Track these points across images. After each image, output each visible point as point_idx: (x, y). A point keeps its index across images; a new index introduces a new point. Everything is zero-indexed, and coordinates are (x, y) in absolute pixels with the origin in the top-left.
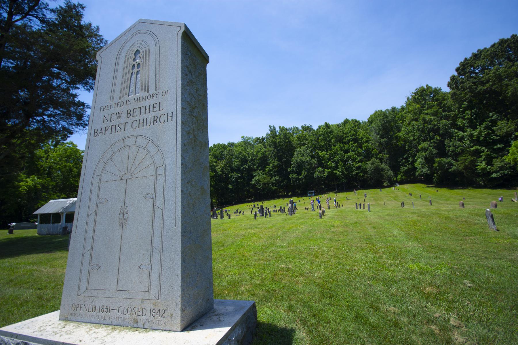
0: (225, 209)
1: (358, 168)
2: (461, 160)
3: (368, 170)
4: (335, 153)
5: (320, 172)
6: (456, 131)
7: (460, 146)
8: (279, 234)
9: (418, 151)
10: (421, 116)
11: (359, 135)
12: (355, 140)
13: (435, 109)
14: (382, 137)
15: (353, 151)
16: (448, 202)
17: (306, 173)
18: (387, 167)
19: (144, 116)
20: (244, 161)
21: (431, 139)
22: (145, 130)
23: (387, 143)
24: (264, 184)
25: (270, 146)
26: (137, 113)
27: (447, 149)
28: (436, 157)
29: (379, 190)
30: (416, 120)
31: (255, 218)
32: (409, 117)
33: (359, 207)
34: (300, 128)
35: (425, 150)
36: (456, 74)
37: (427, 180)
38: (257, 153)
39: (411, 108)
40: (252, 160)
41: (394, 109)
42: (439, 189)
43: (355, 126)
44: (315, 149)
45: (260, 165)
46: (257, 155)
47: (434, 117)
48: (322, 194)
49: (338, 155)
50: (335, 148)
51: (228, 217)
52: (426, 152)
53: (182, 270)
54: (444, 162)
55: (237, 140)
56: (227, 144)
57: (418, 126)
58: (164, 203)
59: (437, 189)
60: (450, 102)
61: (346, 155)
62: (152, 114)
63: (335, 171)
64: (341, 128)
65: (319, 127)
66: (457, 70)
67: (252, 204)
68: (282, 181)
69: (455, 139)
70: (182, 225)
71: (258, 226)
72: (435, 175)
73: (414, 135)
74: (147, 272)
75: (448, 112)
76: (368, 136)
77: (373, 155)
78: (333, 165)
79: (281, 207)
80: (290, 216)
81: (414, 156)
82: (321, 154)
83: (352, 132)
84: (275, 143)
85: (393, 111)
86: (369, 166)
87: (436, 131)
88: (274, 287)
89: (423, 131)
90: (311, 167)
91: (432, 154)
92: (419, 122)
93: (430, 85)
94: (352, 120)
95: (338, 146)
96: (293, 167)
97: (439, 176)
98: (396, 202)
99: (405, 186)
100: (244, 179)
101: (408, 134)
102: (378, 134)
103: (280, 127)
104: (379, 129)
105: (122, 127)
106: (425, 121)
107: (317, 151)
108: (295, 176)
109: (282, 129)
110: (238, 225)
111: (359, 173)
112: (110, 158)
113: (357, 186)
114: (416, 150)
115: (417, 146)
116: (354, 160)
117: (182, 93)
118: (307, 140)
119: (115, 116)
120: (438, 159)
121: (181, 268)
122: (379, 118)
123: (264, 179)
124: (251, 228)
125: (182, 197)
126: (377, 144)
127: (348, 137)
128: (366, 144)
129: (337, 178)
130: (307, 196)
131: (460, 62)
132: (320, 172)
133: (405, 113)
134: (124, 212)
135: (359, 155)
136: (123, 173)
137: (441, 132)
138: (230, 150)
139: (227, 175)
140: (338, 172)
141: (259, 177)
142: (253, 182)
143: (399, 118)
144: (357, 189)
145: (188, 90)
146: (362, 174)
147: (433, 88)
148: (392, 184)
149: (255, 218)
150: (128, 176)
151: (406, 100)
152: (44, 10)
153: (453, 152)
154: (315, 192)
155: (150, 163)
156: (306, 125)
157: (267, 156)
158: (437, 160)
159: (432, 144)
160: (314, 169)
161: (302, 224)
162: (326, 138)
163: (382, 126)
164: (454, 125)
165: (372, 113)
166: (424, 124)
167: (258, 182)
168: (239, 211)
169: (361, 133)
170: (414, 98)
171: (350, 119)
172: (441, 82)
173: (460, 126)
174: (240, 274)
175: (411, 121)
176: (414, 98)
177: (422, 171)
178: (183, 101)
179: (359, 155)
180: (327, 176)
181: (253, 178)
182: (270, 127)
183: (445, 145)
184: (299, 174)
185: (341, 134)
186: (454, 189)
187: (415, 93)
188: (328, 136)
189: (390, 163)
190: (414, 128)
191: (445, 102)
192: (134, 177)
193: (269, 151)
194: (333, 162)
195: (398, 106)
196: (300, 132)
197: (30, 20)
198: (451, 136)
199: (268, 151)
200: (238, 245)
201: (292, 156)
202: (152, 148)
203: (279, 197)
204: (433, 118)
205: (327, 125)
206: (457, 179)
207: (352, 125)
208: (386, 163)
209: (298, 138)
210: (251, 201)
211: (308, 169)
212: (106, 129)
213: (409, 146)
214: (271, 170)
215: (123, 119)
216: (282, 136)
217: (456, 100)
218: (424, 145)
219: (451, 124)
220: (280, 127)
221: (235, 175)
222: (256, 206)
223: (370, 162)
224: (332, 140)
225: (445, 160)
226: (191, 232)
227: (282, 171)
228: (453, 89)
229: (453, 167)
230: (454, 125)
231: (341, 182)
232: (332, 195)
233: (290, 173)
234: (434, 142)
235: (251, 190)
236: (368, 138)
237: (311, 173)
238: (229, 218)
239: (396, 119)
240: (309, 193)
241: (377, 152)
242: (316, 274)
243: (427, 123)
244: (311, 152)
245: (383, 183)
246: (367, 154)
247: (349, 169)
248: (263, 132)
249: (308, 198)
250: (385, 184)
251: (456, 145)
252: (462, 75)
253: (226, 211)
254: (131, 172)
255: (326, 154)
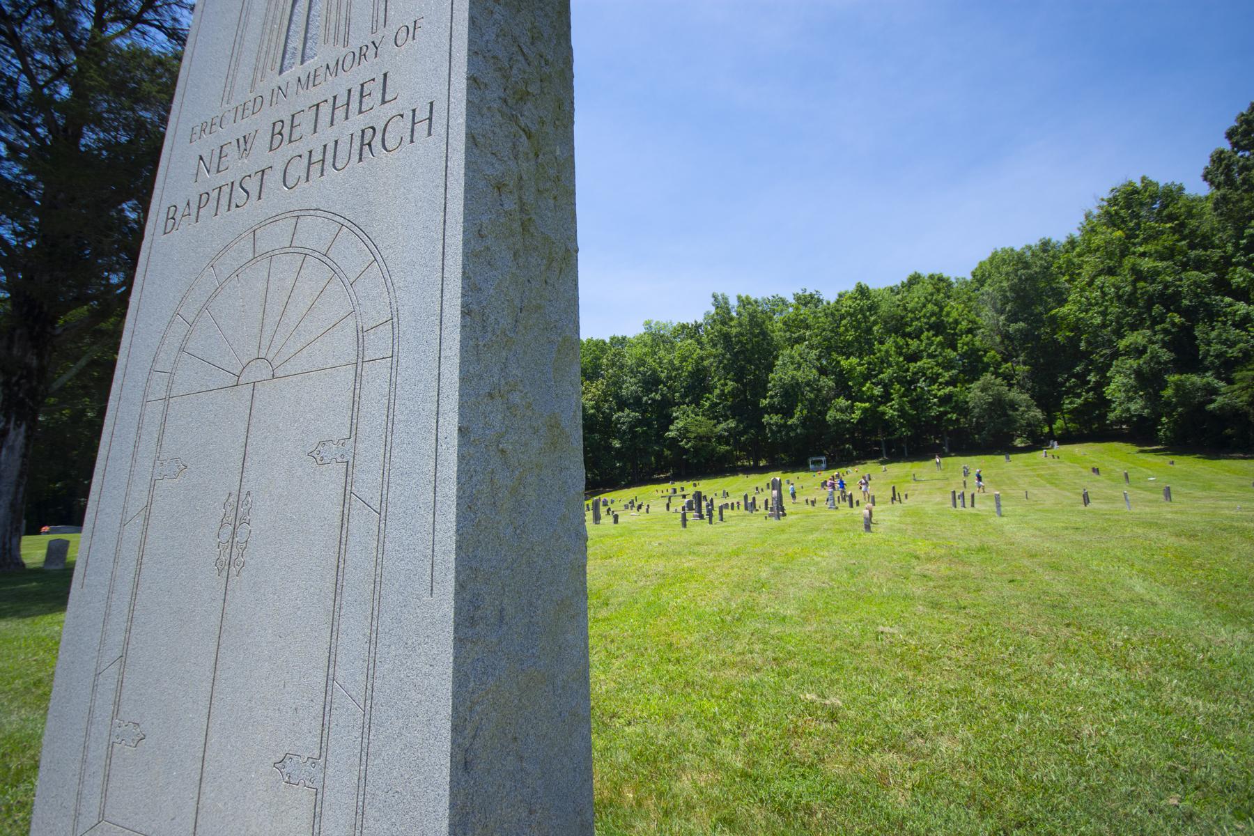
0: (602, 497)
1: (946, 400)
2: (1241, 380)
3: (971, 405)
4: (882, 362)
5: (842, 411)
6: (1228, 300)
7: (1239, 342)
8: (764, 575)
9: (1116, 355)
10: (1128, 262)
11: (948, 314)
12: (938, 328)
13: (1168, 240)
14: (1013, 318)
15: (930, 356)
16: (1213, 493)
17: (805, 412)
18: (1026, 396)
19: (327, 134)
20: (651, 382)
21: (1155, 322)
22: (328, 188)
23: (1026, 336)
24: (699, 438)
25: (714, 345)
26: (304, 126)
27: (1203, 348)
28: (1167, 371)
29: (1003, 457)
30: (1111, 272)
31: (684, 525)
32: (1090, 264)
33: (959, 502)
34: (791, 300)
35: (1139, 352)
36: (1226, 146)
37: (1140, 433)
38: (681, 362)
39: (1097, 240)
40: (669, 378)
41: (1045, 245)
42: (1176, 458)
43: (938, 290)
44: (829, 349)
45: (689, 390)
46: (681, 368)
47: (1165, 264)
48: (847, 466)
49: (890, 365)
50: (884, 348)
51: (611, 519)
52: (1139, 358)
53: (452, 817)
54: (1192, 384)
55: (632, 329)
56: (608, 341)
57: (1118, 288)
58: (385, 484)
59: (1170, 458)
60: (1209, 221)
61: (912, 365)
62: (357, 122)
63: (882, 408)
64: (899, 297)
65: (840, 296)
66: (1230, 135)
67: (668, 487)
68: (742, 434)
69: (1224, 323)
70: (461, 587)
71: (696, 549)
72: (1164, 420)
73: (1104, 314)
74: (306, 796)
75: (1205, 249)
76: (972, 316)
77: (988, 365)
78: (878, 391)
79: (746, 497)
80: (773, 522)
81: (1103, 369)
82: (845, 364)
83: (929, 306)
84: (726, 337)
85: (1045, 251)
86: (975, 394)
87: (1170, 300)
88: (799, 787)
89: (1131, 301)
90: (817, 396)
91: (1159, 363)
92: (1119, 278)
93: (1154, 178)
94: (931, 277)
95: (889, 344)
96: (772, 397)
97: (1176, 422)
98: (1056, 490)
99: (1077, 449)
100: (649, 425)
101: (1087, 311)
102: (1001, 312)
103: (739, 298)
104: (1005, 297)
105: (252, 185)
106: (1138, 275)
107: (834, 355)
108: (776, 418)
109: (744, 302)
110: (638, 536)
111: (946, 413)
112: (205, 307)
113: (941, 445)
114: (1108, 351)
115: (1110, 341)
116: (933, 380)
117: (472, 20)
118: (808, 327)
119: (232, 151)
120: (1177, 377)
121: (452, 806)
122: (1004, 269)
123: (699, 425)
124: (679, 554)
125: (462, 458)
126: (998, 339)
127: (918, 319)
128: (966, 338)
129: (887, 426)
130: (808, 470)
131: (1236, 114)
132: (842, 411)
133: (1080, 255)
134: (237, 514)
135: (948, 365)
136: (245, 361)
137: (1186, 302)
138: (615, 355)
139: (608, 418)
140: (889, 411)
141: (686, 422)
142: (671, 434)
143: (1060, 268)
144: (943, 455)
145: (497, 16)
146: (954, 416)
147: (1161, 185)
148: (1038, 442)
149: (684, 525)
150: (260, 371)
151: (1083, 219)
152: (174, 7)
153: (1217, 356)
154: (827, 461)
155: (342, 314)
156: (805, 290)
157: (705, 368)
158: (1173, 378)
159: (1159, 337)
160: (826, 403)
161: (822, 548)
162: (859, 323)
163: (1012, 288)
164: (1222, 285)
165: (985, 255)
166: (1134, 282)
167: (684, 432)
168: (636, 504)
169: (954, 309)
170: (1108, 213)
171: (925, 272)
172: (1185, 169)
173: (1238, 286)
174: (669, 718)
175: (1095, 277)
176: (1108, 213)
177: (1128, 410)
178: (473, 53)
179: (948, 365)
180: (860, 421)
181: (672, 422)
182: (715, 297)
183: (1196, 338)
184: (788, 413)
185: (900, 312)
186: (1218, 458)
187: (1109, 201)
188: (865, 317)
189: (1033, 387)
190: (1104, 294)
191: (1194, 223)
192: (279, 373)
193: (711, 356)
194: (876, 384)
195: (1059, 237)
196: (791, 310)
197: (144, 33)
198: (1212, 315)
199: (708, 357)
200: (649, 604)
201: (770, 368)
202: (351, 254)
203: (734, 471)
204: (1160, 265)
205: (863, 291)
206: (1229, 431)
207: (930, 289)
208: (1022, 387)
209: (785, 323)
210: (666, 480)
211: (812, 402)
212: (204, 198)
213: (1089, 343)
214: (717, 404)
215: (261, 155)
216: (745, 319)
217: (1227, 216)
218: (1136, 338)
219: (1213, 281)
220: (739, 298)
221: (626, 416)
222: (679, 492)
223: (979, 383)
224: (875, 328)
225: (1195, 378)
226: (501, 619)
227: (745, 406)
228: (1218, 188)
229: (1220, 399)
230: (1222, 285)
231: (897, 435)
232: (870, 468)
233: (765, 410)
234: (1166, 332)
235: (667, 452)
236: (973, 322)
237: (820, 413)
238: (616, 521)
239: (1054, 269)
240: (813, 463)
241: (999, 357)
242: (944, 744)
243: (1145, 280)
244: (819, 358)
245: (1012, 438)
246: (970, 363)
247: (919, 402)
248: (696, 311)
249: (810, 475)
250: (1018, 443)
251: (1227, 340)
252: (1244, 148)
253: (605, 504)
254: (270, 356)
255: (860, 364)
